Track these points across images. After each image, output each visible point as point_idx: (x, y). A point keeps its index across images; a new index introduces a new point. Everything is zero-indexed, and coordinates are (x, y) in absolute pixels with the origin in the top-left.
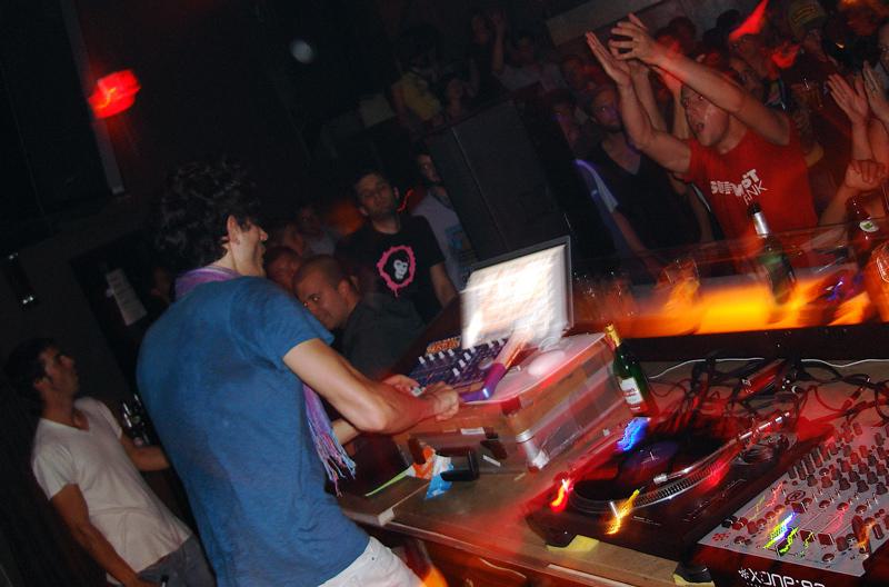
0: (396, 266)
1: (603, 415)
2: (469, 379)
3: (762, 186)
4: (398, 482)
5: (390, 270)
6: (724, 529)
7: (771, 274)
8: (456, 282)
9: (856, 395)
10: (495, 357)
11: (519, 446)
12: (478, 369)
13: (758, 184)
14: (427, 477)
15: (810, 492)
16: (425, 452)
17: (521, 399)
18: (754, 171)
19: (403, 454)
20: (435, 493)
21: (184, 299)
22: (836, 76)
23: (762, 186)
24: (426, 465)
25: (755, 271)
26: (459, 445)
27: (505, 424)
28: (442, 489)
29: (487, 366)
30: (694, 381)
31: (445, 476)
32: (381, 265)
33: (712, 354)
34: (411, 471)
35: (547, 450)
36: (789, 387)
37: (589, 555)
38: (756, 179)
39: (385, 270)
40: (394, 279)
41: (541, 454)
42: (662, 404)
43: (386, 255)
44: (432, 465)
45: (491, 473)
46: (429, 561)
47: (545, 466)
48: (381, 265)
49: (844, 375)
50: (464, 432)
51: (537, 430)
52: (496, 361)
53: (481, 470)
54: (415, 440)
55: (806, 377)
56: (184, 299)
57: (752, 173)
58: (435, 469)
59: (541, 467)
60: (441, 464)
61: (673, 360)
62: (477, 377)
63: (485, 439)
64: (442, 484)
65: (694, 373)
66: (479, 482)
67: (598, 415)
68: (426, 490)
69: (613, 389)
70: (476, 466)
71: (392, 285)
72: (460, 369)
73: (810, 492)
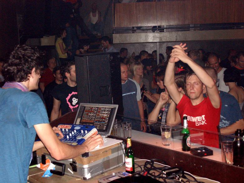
0: (73, 100)
1: (111, 168)
2: (72, 140)
3: (205, 122)
5: (71, 101)
8: (148, 112)
10: (83, 136)
12: (76, 139)
13: (204, 121)
14: (44, 169)
16: (46, 161)
18: (204, 116)
19: (38, 159)
20: (46, 176)
23: (205, 122)
27: (81, 161)
28: (49, 175)
29: (80, 138)
30: (145, 166)
32: (68, 99)
33: (154, 159)
34: (39, 166)
35: (92, 173)
36: (179, 179)
38: (204, 119)
39: (69, 101)
40: (72, 105)
41: (90, 174)
43: (70, 95)
44: (48, 165)
45: (68, 175)
47: (89, 179)
48: (68, 99)
52: (83, 138)
53: (66, 173)
54: (45, 155)
55: (185, 177)
57: (203, 116)
59: (88, 178)
60: (52, 167)
61: (140, 158)
62: (75, 141)
63: (72, 163)
64: (49, 173)
65: (145, 164)
66: (63, 177)
67: (109, 167)
68: (42, 174)
70: (64, 171)
71: (71, 107)
72: (69, 137)
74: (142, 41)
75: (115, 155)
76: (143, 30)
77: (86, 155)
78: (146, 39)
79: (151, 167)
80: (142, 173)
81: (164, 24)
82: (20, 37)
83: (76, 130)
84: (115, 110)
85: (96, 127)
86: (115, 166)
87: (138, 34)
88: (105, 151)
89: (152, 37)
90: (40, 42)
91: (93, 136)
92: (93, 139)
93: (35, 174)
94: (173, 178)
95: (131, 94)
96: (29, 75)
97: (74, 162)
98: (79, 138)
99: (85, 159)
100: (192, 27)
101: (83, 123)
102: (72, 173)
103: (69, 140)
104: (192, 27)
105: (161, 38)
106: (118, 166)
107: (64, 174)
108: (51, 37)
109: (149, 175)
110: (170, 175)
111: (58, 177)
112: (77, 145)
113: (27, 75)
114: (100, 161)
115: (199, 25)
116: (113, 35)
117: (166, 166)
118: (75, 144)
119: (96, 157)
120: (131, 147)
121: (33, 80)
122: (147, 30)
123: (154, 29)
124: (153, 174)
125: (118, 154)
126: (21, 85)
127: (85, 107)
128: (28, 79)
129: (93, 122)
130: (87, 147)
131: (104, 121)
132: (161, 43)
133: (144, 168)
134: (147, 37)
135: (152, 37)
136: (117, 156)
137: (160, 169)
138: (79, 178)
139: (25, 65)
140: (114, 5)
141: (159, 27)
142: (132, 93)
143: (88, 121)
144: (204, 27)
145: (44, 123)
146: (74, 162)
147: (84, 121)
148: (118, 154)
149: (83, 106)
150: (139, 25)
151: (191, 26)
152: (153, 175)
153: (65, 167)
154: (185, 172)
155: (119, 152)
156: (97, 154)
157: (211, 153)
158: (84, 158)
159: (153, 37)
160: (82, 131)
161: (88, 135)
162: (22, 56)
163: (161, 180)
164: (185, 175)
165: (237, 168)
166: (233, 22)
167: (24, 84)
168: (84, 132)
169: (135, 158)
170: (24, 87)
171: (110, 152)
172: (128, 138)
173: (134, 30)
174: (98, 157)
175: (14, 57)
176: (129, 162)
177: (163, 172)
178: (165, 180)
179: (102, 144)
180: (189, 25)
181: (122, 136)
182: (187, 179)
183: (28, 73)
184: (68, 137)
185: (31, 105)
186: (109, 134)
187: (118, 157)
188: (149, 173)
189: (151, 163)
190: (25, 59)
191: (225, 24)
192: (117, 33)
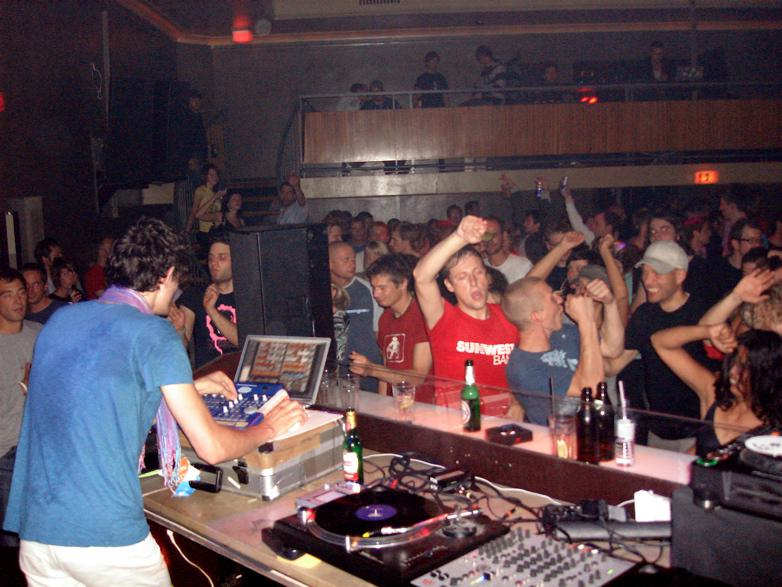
1: (319, 475)
2: (235, 417)
4: (148, 478)
6: (432, 578)
7: (274, 474)
9: (513, 511)
10: (259, 408)
11: (260, 478)
15: (494, 567)
17: (274, 445)
25: (447, 406)
28: (188, 492)
30: (392, 468)
31: (193, 484)
33: (410, 453)
35: (281, 486)
36: (465, 493)
37: (311, 571)
42: (367, 479)
46: (492, 443)
49: (505, 495)
51: (279, 469)
52: (258, 411)
53: (223, 487)
55: (475, 489)
59: (272, 498)
60: (194, 474)
62: (242, 417)
64: (188, 488)
66: (219, 497)
69: (334, 457)
70: (220, 484)
73: (494, 567)
74: (364, 194)
75: (328, 445)
76: (366, 170)
77: (267, 448)
78: (372, 189)
79: (405, 470)
80: (386, 484)
81: (410, 156)
82: (98, 186)
83: (243, 395)
84: (324, 349)
85: (284, 387)
86: (328, 471)
87: (355, 178)
88: (306, 439)
89: (383, 185)
90: (141, 199)
91: (283, 405)
92: (283, 411)
93: (156, 491)
94: (452, 492)
95: (355, 314)
96: (162, 279)
97: (242, 464)
98: (250, 411)
99: (266, 457)
100: (469, 164)
101: (257, 377)
102: (238, 486)
103: (228, 417)
104: (469, 164)
105: (404, 187)
106: (332, 469)
107: (220, 490)
108: (165, 186)
109: (401, 488)
110: (445, 486)
111: (207, 497)
112: (247, 427)
113: (157, 279)
114: (296, 459)
115: (484, 160)
116: (302, 180)
117: (436, 468)
118: (242, 424)
119: (288, 451)
120: (355, 429)
121: (164, 293)
122: (374, 169)
123: (389, 168)
124: (411, 484)
125: (334, 443)
126: (140, 299)
127: (258, 344)
128: (158, 288)
129: (276, 374)
130: (273, 429)
131: (302, 373)
132: (404, 197)
133: (390, 471)
134: (374, 184)
135: (383, 185)
136: (331, 447)
137: (423, 473)
138: (254, 497)
139: (158, 257)
140: (303, 118)
141: (402, 163)
142: (359, 311)
143: (267, 374)
144: (495, 163)
145: (183, 382)
146: (242, 464)
147: (258, 373)
148: (334, 443)
149: (254, 341)
150: (358, 159)
151: (467, 161)
152: (410, 488)
153: (221, 475)
154: (477, 478)
155: (336, 439)
156: (291, 445)
157: (527, 436)
158: (264, 454)
159: (388, 184)
160: (256, 397)
161: (269, 405)
162: (152, 240)
163: (429, 496)
164: (478, 485)
165: (585, 467)
166: (555, 153)
167: (147, 297)
168: (261, 399)
169: (364, 450)
170: (145, 305)
171: (318, 438)
172: (349, 410)
173: (346, 170)
174: (292, 452)
175: (133, 239)
176: (351, 462)
177: (432, 479)
178: (437, 497)
179: (304, 420)
180: (463, 158)
181: (339, 405)
182: (482, 492)
183: (159, 274)
184: (225, 410)
185: (158, 343)
186: (313, 402)
187: (333, 449)
188: (401, 484)
189: (405, 462)
190: (155, 246)
191: (539, 157)
192: (310, 177)
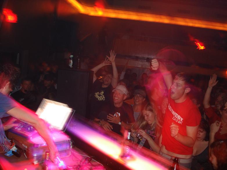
11: (33, 157)
13: (181, 121)
21: (10, 95)
22: (216, 75)
24: (12, 147)
26: (21, 147)
31: (13, 152)
33: (92, 157)
50: (23, 145)
56: (10, 95)
58: (12, 149)
60: (14, 149)
64: (11, 153)
